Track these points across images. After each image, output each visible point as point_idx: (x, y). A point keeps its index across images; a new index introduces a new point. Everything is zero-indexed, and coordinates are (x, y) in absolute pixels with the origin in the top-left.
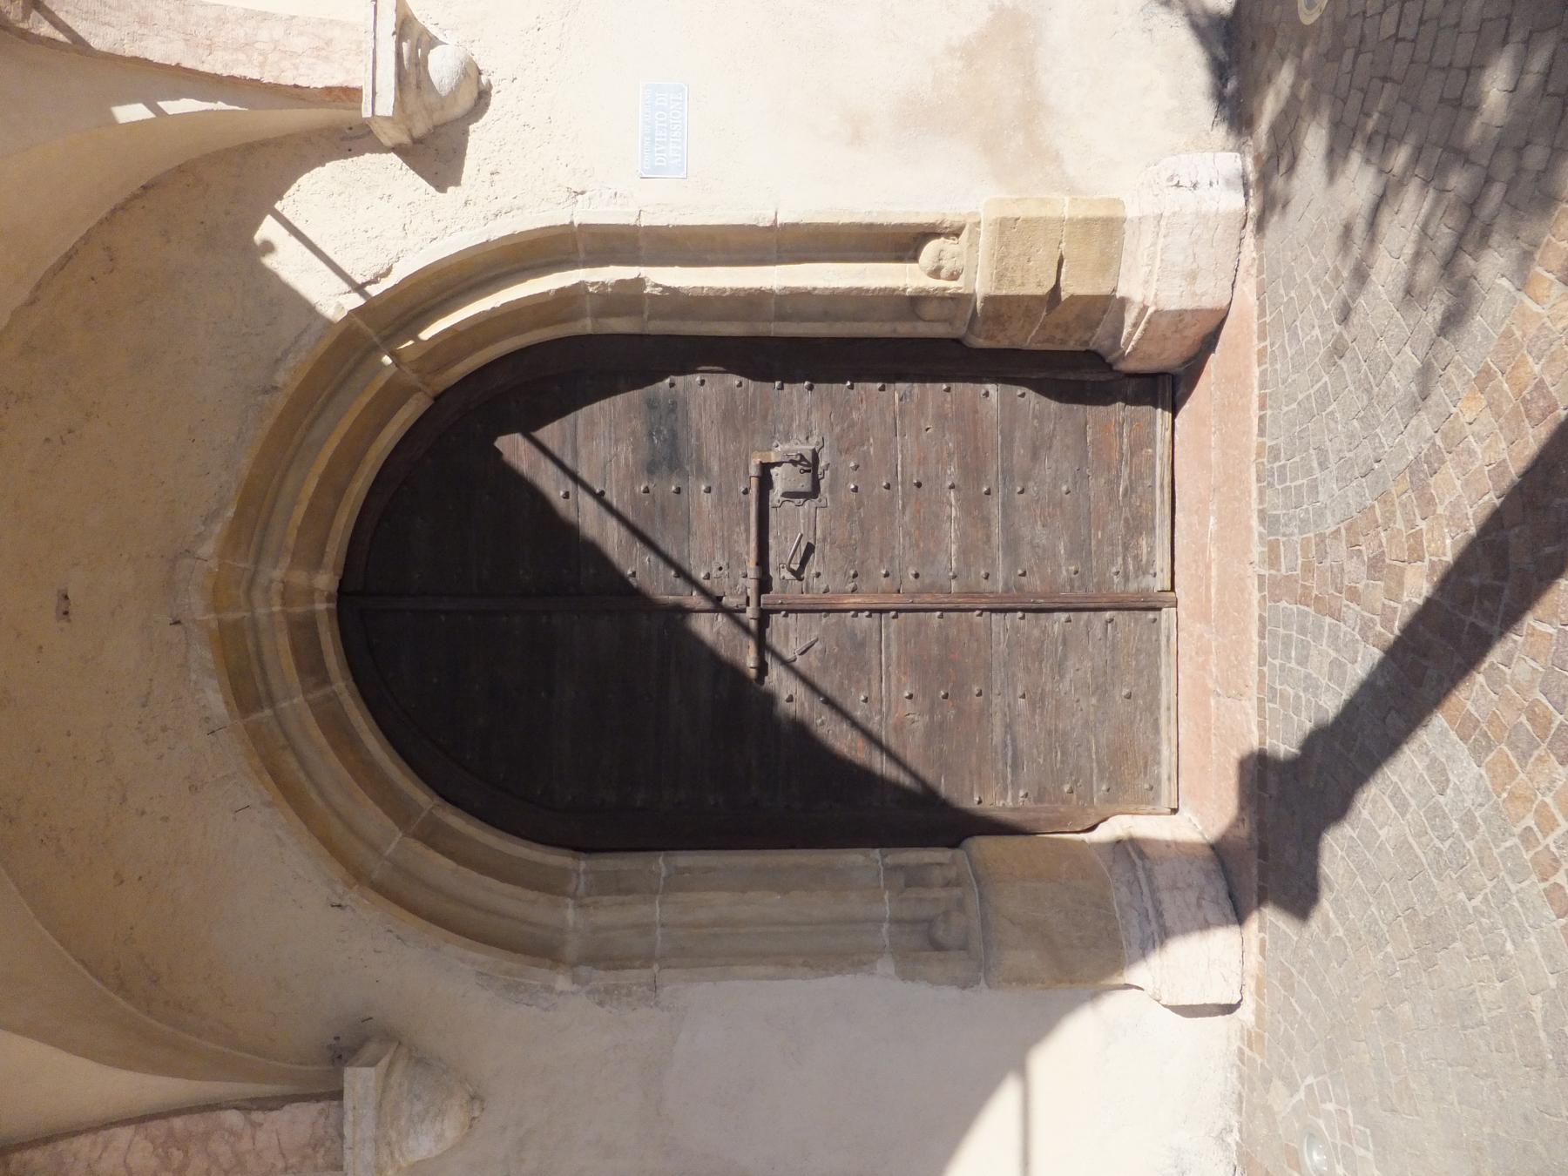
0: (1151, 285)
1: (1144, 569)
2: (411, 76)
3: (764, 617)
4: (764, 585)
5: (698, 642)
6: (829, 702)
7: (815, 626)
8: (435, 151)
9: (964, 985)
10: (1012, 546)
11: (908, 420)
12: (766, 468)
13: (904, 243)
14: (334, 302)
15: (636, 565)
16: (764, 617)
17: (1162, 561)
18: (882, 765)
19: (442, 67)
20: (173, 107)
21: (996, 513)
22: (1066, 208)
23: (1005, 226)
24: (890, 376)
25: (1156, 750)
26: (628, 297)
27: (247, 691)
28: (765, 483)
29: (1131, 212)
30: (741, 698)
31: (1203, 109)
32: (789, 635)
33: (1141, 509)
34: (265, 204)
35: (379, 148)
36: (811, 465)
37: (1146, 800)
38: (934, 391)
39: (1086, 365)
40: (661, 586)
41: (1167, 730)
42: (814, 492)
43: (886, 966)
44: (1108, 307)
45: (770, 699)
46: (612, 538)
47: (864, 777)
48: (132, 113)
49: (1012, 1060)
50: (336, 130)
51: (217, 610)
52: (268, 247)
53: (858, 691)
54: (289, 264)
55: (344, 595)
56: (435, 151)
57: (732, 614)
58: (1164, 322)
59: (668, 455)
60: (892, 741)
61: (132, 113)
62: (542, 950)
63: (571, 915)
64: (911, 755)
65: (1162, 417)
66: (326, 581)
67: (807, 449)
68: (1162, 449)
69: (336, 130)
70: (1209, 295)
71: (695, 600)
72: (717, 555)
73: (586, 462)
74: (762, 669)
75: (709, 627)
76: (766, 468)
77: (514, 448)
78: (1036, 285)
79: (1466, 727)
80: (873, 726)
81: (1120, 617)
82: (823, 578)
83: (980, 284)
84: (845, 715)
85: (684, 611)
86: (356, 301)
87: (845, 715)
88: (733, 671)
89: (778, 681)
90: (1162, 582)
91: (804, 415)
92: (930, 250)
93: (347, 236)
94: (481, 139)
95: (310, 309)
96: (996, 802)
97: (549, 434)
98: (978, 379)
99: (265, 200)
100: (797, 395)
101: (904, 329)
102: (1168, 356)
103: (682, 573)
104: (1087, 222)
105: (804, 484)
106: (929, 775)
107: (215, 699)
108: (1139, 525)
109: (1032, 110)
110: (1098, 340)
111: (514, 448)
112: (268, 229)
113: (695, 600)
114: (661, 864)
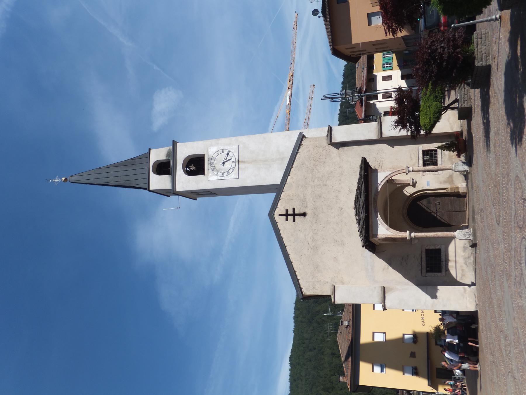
0: (461, 191)
2: (413, 182)
8: (414, 185)
13: (444, 189)
14: (408, 195)
19: (414, 181)
22: (455, 187)
30: (435, 218)
32: (438, 214)
38: (448, 198)
40: (430, 211)
44: (458, 188)
46: (425, 208)
50: (409, 185)
51: (476, 372)
53: (445, 219)
54: (405, 193)
56: (414, 185)
58: (408, 71)
59: (429, 202)
69: (409, 185)
72: (433, 209)
73: (424, 203)
75: (433, 213)
77: (418, 203)
79: (452, 130)
91: (439, 200)
93: (409, 191)
96: (454, 224)
99: (403, 189)
100: (438, 198)
107: (402, 217)
108: (464, 206)
111: (418, 203)
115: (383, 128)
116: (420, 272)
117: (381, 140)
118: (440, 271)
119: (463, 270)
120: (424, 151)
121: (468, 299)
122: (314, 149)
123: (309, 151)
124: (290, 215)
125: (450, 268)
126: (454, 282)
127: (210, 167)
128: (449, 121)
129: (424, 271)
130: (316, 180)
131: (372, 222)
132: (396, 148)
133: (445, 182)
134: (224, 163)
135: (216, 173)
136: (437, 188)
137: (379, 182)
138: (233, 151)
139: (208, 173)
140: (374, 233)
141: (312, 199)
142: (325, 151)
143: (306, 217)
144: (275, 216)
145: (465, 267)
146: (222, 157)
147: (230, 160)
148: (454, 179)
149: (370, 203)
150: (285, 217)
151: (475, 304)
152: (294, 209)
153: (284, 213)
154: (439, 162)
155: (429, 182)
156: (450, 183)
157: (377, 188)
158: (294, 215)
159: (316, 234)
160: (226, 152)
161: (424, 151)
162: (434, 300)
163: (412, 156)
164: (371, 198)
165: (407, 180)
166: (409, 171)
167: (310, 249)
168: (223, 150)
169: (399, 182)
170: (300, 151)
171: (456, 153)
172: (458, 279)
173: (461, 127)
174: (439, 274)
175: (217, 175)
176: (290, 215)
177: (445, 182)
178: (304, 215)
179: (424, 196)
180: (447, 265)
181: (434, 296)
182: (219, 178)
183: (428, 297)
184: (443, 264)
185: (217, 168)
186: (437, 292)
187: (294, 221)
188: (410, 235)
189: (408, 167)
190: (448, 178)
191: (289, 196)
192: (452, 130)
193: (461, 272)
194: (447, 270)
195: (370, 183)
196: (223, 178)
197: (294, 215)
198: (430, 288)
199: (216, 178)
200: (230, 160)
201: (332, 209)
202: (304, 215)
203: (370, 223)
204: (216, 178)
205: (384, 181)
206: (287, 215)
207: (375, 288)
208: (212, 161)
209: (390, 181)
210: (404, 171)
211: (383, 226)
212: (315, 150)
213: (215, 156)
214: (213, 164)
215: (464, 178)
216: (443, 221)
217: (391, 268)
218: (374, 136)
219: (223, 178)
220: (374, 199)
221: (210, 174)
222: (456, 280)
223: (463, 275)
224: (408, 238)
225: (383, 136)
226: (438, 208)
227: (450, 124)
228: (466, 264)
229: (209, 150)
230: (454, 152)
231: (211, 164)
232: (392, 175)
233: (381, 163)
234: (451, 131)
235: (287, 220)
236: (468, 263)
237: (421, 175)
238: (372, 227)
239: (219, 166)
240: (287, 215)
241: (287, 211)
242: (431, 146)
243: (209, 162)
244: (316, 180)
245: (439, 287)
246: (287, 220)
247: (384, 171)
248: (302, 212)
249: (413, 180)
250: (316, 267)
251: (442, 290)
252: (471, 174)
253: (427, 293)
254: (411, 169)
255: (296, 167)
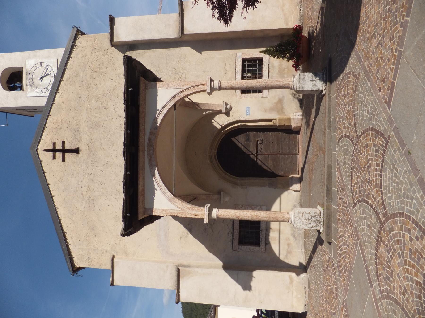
0: (294, 124)
1: (296, 151)
2: (226, 108)
3: (257, 155)
4: (257, 152)
5: (250, 157)
6: (263, 163)
7: (262, 156)
8: (227, 113)
9: (275, 188)
10: (282, 148)
11: (272, 136)
12: (257, 141)
13: (270, 121)
14: (219, 127)
15: (245, 150)
16: (257, 155)
17: (298, 150)
18: (268, 170)
19: (228, 107)
20: (207, 112)
21: (280, 145)
22: (285, 118)
23: (279, 119)
24: (270, 132)
25: (296, 169)
26: (245, 125)
27: (211, 162)
28: (257, 142)
29: (291, 118)
30: (255, 163)
31: (299, 108)
32: (260, 157)
33: (296, 145)
34: (213, 119)
35: (222, 113)
36: (262, 140)
37: (296, 174)
39: (288, 131)
40: (247, 152)
41: (298, 167)
42: (262, 143)
43: (267, 186)
44: (289, 120)
45: (258, 163)
46: (242, 147)
47: (267, 171)
48: (204, 113)
49: (279, 195)
50: (219, 112)
52: (213, 122)
53: (268, 164)
54: (215, 124)
55: (217, 153)
56: (227, 113)
57: (254, 155)
59: (248, 139)
60: (269, 167)
61: (204, 113)
62: (237, 184)
63: (239, 182)
64: (271, 169)
65: (298, 135)
66: (216, 151)
67: (261, 139)
68: (298, 139)
69: (219, 112)
70: (299, 125)
71: (250, 153)
72: (253, 150)
74: (257, 160)
75: (252, 156)
76: (257, 141)
77: (233, 139)
78: (283, 124)
79: (287, 24)
80: (268, 165)
81: (293, 156)
82: (263, 151)
83: (278, 124)
84: (265, 165)
85: (249, 155)
86: (221, 127)
87: (265, 165)
88: (254, 160)
89: (258, 161)
90: (298, 152)
91: (261, 136)
92: (273, 121)
93: (220, 121)
94: (231, 112)
95: (216, 128)
96: (280, 173)
97: (236, 138)
98: (279, 132)
99: (213, 118)
100: (261, 134)
101: (271, 127)
102: (297, 130)
103: (249, 151)
104: (287, 119)
105: (261, 142)
106: (273, 170)
107: (209, 161)
108: (296, 146)
109: (282, 108)
110: (290, 128)
111: (233, 139)
112: (213, 121)
113: (250, 153)
114: (247, 178)
115: (185, 19)
116: (230, 243)
117: (183, 40)
118: (257, 243)
119: (289, 245)
120: (244, 61)
121: (295, 294)
122: (92, 53)
123: (86, 55)
124: (59, 151)
125: (271, 240)
126: (277, 265)
127: (28, 81)
128: (283, 10)
129: (236, 242)
130: (93, 101)
131: (144, 185)
132: (206, 54)
133: (272, 110)
134: (42, 78)
135: (34, 89)
136: (260, 118)
137: (159, 107)
138: (51, 65)
139: (26, 89)
140: (147, 206)
141: (87, 129)
142: (106, 56)
143: (80, 155)
144: (39, 151)
145: (292, 239)
146: (40, 72)
147: (48, 74)
148: (285, 106)
149: (141, 148)
150: (51, 154)
151: (304, 302)
152: (63, 142)
153: (51, 147)
154: (203, 217)
155: (249, 109)
156: (278, 112)
157: (155, 120)
158: (64, 151)
159: (92, 180)
160: (44, 65)
161: (244, 61)
162: (247, 292)
163: (228, 67)
164: (144, 138)
165: (219, 105)
166: (213, 89)
167: (84, 202)
168: (41, 64)
169: (206, 108)
170: (73, 55)
171: (291, 63)
172: (282, 258)
173: (300, 20)
174: (256, 248)
175: (36, 91)
176: (59, 151)
177: (272, 110)
178: (76, 151)
179: (242, 129)
180: (267, 235)
181: (247, 287)
182: (38, 95)
183: (239, 288)
184: (263, 233)
185: (35, 83)
186: (251, 280)
187: (64, 160)
188: (210, 214)
189: (212, 80)
190: (276, 103)
191: (57, 122)
192: (287, 24)
193: (286, 247)
194: (268, 243)
195: (141, 109)
196: (42, 95)
197: (64, 151)
198: (243, 274)
199: (35, 94)
200: (48, 74)
201: (113, 144)
202: (76, 151)
203: (140, 188)
204: (35, 94)
205: (169, 106)
206: (54, 151)
207: (167, 267)
208: (31, 76)
209: (183, 105)
210: (204, 88)
211: (164, 194)
212: (94, 55)
213: (33, 70)
214: (32, 78)
215: (298, 104)
216: (265, 167)
217: (191, 236)
218: (171, 32)
219: (42, 95)
220: (150, 140)
221: (29, 90)
222: (278, 259)
223: (289, 252)
224: (206, 221)
225: (185, 32)
226: (259, 148)
227: (285, 15)
228: (294, 236)
229: (27, 63)
230: (289, 59)
231: (29, 79)
232: (186, 93)
233: (183, 76)
234: (285, 27)
235: (54, 158)
236: (296, 235)
237: (239, 97)
238: (143, 195)
239: (37, 81)
240: (54, 151)
241: (54, 144)
242: (254, 53)
243: (28, 76)
244: (93, 101)
245: (257, 274)
246: (54, 158)
247: (169, 87)
248: (74, 147)
249: (226, 104)
250: (93, 229)
251: (259, 276)
252: (330, 98)
253: (237, 281)
254: (216, 84)
255: (67, 80)
